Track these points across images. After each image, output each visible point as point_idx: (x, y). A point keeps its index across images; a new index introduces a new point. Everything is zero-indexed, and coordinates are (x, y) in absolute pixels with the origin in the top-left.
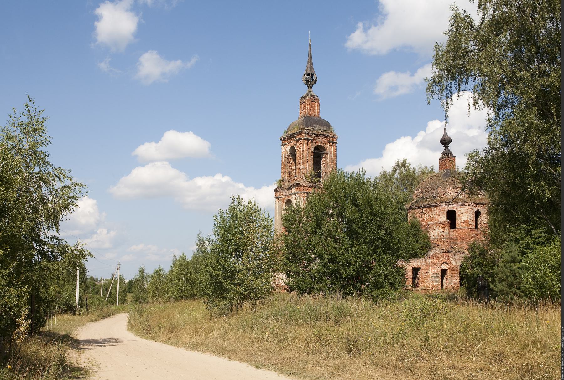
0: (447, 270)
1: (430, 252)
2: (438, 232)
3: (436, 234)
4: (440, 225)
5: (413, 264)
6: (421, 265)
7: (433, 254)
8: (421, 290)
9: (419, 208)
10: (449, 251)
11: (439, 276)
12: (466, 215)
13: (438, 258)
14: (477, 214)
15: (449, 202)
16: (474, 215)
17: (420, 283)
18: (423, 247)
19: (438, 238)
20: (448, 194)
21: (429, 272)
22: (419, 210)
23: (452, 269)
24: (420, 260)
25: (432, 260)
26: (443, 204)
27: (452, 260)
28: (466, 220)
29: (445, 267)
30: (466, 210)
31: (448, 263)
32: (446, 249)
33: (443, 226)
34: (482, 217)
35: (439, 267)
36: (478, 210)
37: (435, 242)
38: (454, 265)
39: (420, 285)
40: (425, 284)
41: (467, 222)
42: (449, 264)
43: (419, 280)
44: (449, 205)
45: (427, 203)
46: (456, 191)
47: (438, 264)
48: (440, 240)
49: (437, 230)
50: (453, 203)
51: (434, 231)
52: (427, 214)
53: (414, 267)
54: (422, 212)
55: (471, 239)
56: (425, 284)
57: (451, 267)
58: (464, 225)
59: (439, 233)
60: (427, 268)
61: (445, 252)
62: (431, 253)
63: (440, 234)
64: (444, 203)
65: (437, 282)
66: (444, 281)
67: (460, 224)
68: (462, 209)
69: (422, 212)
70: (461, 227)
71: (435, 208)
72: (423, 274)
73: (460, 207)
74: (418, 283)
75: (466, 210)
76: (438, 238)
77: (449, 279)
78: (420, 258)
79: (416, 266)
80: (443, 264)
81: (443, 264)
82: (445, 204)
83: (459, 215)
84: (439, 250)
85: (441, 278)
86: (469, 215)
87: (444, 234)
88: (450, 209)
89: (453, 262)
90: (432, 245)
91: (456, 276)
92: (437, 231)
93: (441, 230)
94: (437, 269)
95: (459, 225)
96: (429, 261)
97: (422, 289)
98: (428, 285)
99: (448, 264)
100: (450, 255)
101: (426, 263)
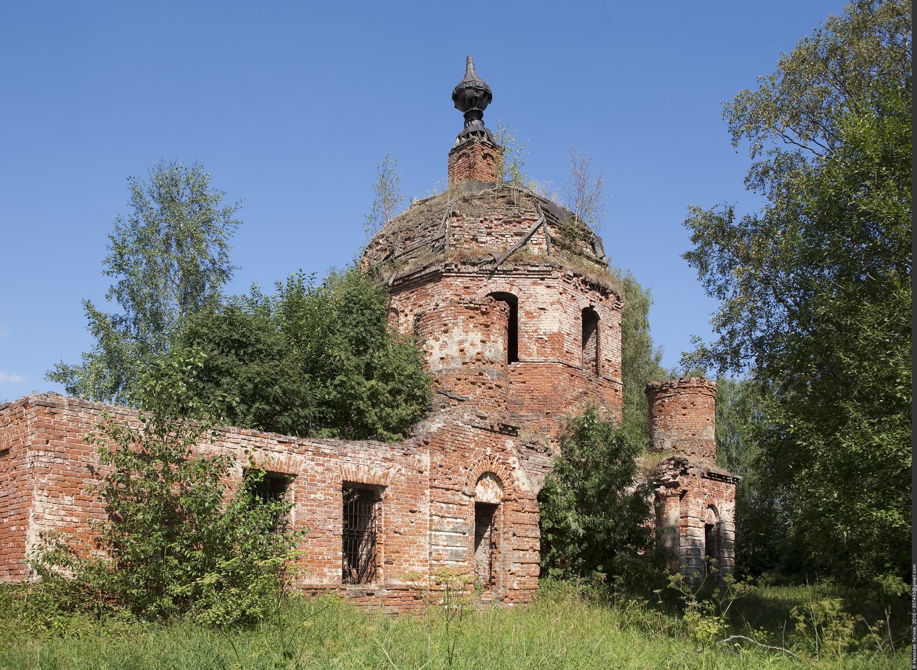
0: (494, 507)
1: (427, 423)
2: (461, 342)
3: (453, 350)
4: (472, 313)
5: (350, 466)
6: (386, 475)
7: (442, 431)
8: (386, 592)
10: (506, 426)
11: (465, 529)
12: (556, 314)
13: (462, 450)
14: (589, 319)
15: (494, 261)
16: (580, 321)
17: (382, 558)
18: (399, 392)
19: (460, 366)
20: (488, 238)
21: (425, 508)
23: (514, 506)
24: (381, 451)
25: (439, 458)
26: (470, 269)
27: (517, 465)
28: (556, 330)
29: (488, 493)
30: (557, 297)
31: (503, 477)
32: (494, 417)
33: (483, 319)
34: (602, 336)
35: (466, 489)
36: (592, 307)
37: (446, 386)
38: (523, 488)
39: (381, 571)
40: (405, 565)
41: (556, 339)
42: (506, 483)
43: (373, 545)
44: (492, 273)
45: (407, 269)
46: (515, 230)
47: (464, 479)
48: (472, 378)
49: (457, 333)
50: (510, 267)
51: (443, 338)
52: (407, 311)
53: (351, 478)
55: (570, 404)
56: (405, 565)
57: (513, 497)
58: (548, 350)
59: (466, 345)
60: (414, 489)
61: (492, 430)
62: (434, 425)
63: (471, 352)
64: (474, 265)
65: (456, 556)
66: (535, 565)
67: (534, 347)
68: (541, 290)
70: (535, 358)
71: (440, 285)
72: (397, 520)
73: (535, 284)
74: (372, 557)
75: (557, 297)
76: (460, 366)
77: (503, 545)
78: (382, 439)
79: (363, 477)
80: (480, 479)
81: (480, 479)
82: (476, 269)
83: (528, 313)
84: (466, 417)
85: (472, 538)
86: (564, 315)
87: (488, 354)
88: (498, 290)
89: (519, 474)
90: (436, 400)
91: (529, 534)
92: (456, 339)
93: (476, 336)
94: (457, 498)
95: (486, 415)
96: (425, 459)
97: (389, 587)
98: (418, 568)
99: (498, 480)
100: (510, 443)
101: (408, 466)
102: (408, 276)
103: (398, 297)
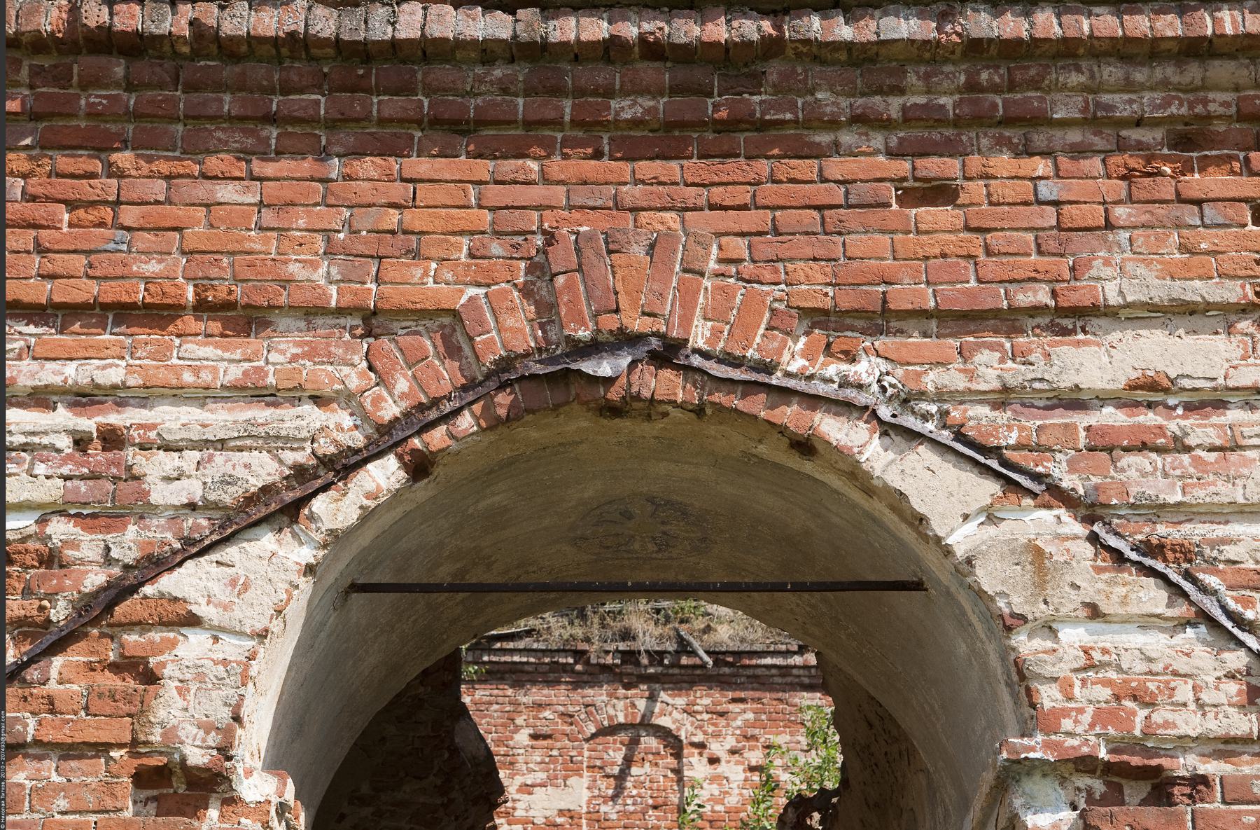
9: (595, 674)
22: (598, 695)
54: (645, 725)
69: (645, 725)
102: (738, 654)
103: (681, 701)
